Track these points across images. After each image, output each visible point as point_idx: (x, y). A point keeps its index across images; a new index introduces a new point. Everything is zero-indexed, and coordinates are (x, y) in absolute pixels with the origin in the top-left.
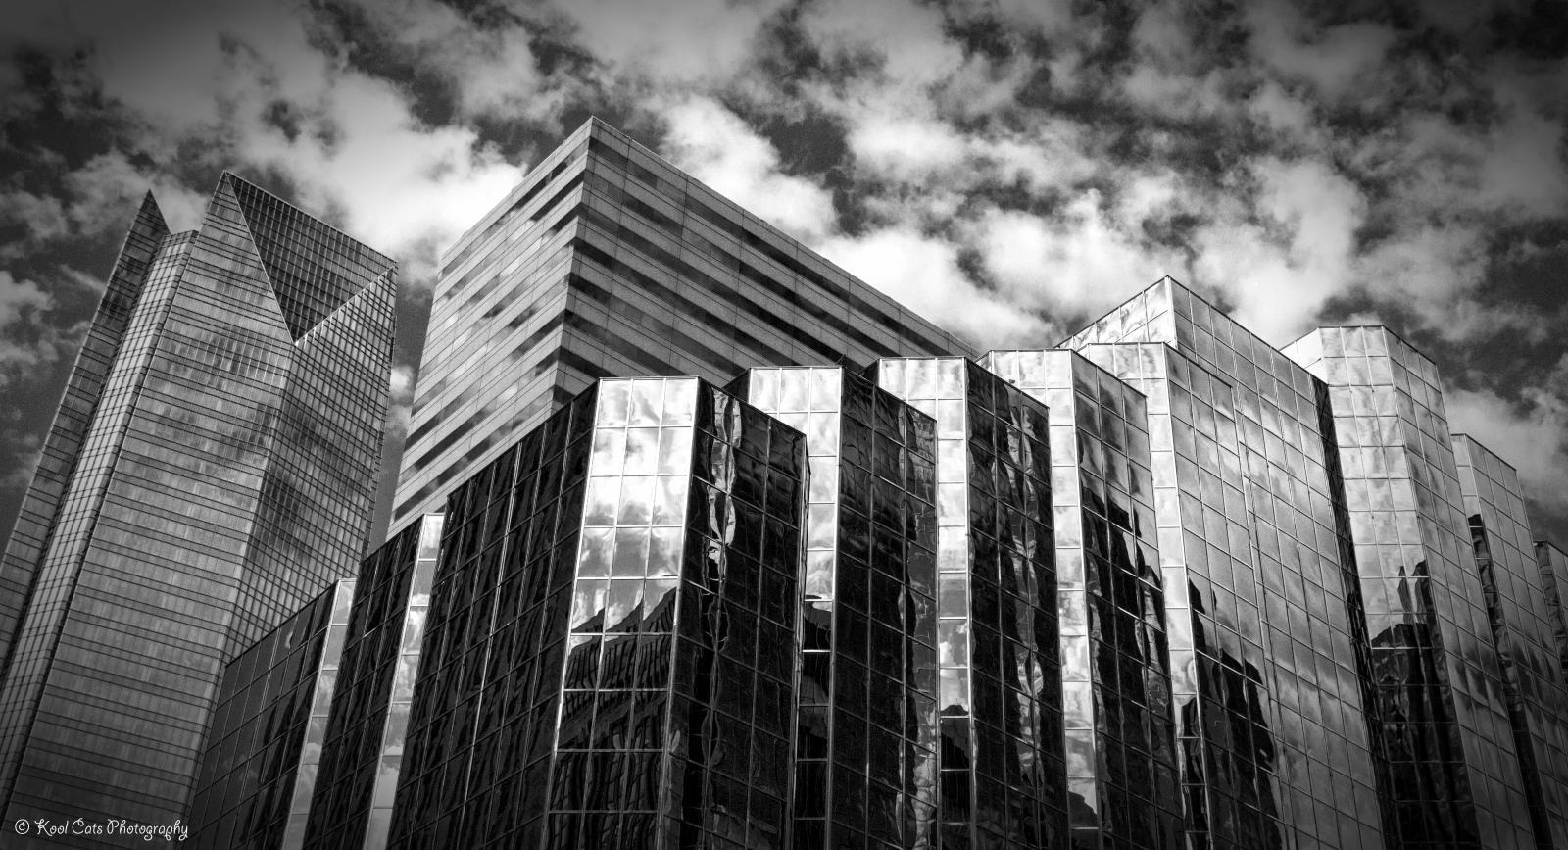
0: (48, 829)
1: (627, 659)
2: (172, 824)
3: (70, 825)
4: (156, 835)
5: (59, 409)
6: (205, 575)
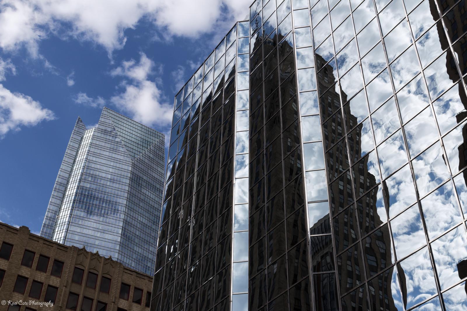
0: (11, 303)
1: (322, 225)
2: (48, 302)
3: (18, 302)
4: (44, 305)
5: (54, 189)
6: (55, 204)
